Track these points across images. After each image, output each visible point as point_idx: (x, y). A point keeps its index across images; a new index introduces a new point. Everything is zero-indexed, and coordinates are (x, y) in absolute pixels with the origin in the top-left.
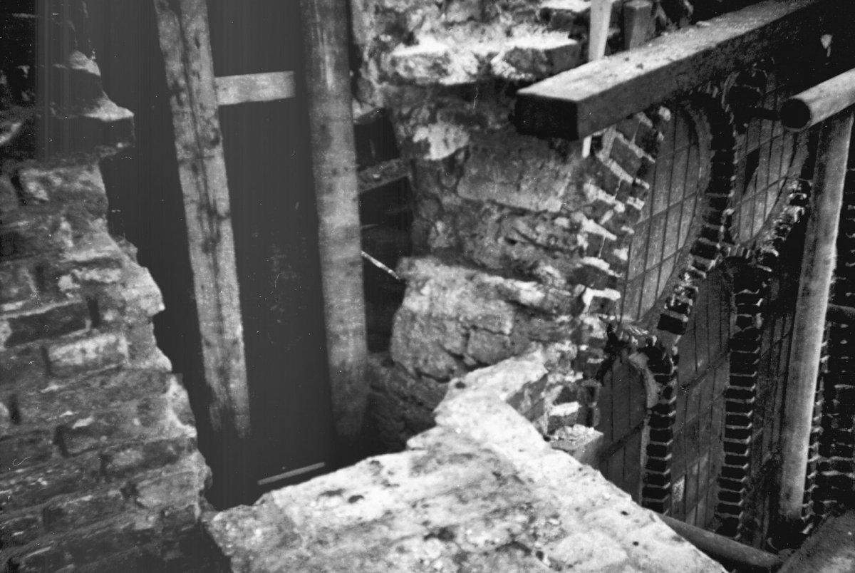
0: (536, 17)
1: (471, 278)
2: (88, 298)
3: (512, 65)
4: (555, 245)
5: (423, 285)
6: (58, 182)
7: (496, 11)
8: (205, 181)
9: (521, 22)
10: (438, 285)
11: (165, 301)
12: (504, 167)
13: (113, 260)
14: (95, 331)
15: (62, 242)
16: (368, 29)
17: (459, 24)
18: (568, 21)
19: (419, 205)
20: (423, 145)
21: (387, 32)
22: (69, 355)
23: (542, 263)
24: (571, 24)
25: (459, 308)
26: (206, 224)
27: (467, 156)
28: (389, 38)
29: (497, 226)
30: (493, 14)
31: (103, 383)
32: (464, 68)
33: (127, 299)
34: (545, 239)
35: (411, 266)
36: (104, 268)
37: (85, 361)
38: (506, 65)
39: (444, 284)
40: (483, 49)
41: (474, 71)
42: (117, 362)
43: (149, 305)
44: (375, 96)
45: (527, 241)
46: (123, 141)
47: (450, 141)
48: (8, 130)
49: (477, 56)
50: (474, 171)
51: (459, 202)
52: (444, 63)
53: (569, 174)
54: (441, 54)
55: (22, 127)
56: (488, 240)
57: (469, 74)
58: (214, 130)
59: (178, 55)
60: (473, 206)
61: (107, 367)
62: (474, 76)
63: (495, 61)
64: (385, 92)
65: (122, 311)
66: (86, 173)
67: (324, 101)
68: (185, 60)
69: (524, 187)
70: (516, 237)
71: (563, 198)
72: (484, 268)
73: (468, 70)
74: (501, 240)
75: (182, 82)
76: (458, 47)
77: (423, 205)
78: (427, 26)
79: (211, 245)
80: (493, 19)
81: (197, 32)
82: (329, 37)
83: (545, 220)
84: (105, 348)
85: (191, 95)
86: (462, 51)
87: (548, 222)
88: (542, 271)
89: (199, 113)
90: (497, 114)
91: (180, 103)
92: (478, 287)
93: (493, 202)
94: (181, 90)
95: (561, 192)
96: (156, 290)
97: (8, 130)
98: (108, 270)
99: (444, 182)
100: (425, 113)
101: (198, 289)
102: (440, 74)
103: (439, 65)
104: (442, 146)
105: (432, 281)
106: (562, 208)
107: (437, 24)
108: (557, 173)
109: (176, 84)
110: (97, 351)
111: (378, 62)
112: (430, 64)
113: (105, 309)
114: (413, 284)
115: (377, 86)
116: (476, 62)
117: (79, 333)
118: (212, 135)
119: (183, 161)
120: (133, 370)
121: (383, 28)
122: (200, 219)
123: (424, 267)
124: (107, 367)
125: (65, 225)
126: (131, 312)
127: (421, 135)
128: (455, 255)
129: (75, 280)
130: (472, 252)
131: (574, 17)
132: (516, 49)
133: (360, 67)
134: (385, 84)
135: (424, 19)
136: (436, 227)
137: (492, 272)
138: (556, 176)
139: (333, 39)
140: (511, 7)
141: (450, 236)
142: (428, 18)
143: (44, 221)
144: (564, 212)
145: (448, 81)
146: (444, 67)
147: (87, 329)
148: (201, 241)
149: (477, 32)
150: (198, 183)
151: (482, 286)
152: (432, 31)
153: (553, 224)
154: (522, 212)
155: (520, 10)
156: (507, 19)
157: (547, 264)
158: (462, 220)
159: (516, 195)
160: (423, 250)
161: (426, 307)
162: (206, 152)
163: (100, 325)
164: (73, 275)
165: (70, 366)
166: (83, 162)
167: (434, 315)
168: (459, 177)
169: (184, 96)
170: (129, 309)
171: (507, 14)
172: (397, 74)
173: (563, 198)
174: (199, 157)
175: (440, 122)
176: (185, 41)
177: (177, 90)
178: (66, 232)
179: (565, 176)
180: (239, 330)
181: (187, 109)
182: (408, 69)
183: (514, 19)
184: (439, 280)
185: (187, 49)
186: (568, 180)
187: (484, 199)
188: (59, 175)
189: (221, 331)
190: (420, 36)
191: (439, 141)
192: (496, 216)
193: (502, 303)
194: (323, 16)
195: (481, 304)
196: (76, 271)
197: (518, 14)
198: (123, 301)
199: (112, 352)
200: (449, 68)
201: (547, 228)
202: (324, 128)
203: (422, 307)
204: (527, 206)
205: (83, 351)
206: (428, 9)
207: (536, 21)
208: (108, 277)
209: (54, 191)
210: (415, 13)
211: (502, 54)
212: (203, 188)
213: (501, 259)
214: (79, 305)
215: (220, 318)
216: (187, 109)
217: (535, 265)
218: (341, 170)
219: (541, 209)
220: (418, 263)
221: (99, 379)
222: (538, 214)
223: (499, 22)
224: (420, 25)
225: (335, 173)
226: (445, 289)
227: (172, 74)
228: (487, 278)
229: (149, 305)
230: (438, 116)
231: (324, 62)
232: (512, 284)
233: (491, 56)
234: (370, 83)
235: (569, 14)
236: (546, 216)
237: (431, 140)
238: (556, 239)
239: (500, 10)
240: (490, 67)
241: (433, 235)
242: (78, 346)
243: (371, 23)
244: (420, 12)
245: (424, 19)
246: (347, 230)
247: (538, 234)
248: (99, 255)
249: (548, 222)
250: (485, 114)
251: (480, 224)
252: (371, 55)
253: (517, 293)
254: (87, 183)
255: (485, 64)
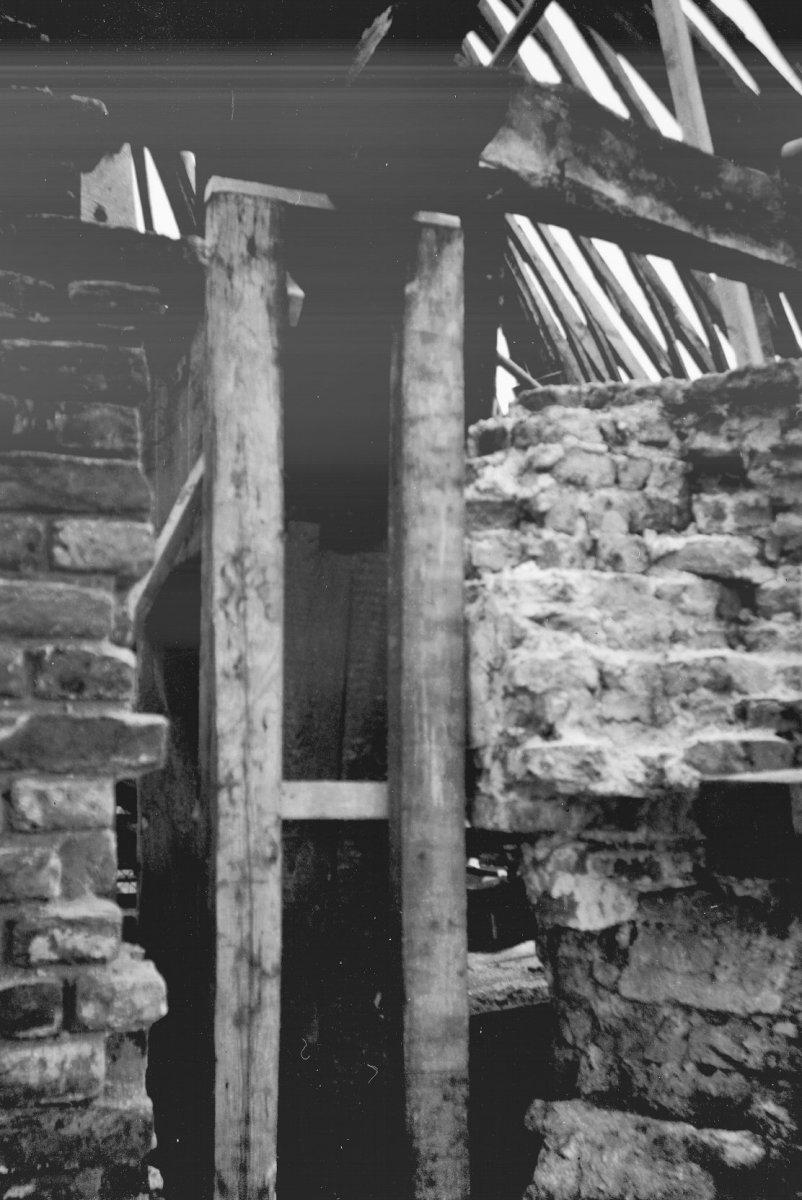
0: (728, 716)
1: (644, 1129)
2: (66, 982)
3: (696, 767)
4: (778, 1068)
5: (567, 1142)
6: (57, 798)
7: (671, 709)
8: (251, 915)
9: (707, 724)
10: (592, 1143)
11: (171, 999)
12: (688, 947)
13: (108, 923)
14: (66, 1035)
15: (47, 887)
16: (492, 722)
17: (619, 722)
18: (773, 714)
19: (561, 1021)
20: (566, 901)
21: (517, 725)
22: (22, 1064)
23: (757, 1097)
24: (778, 717)
25: (625, 1179)
26: (244, 982)
27: (634, 934)
28: (521, 731)
29: (684, 1045)
30: (667, 715)
31: (60, 1124)
32: (625, 773)
33: (118, 988)
34: (759, 1059)
35: (547, 1110)
36: (95, 933)
37: (42, 1079)
38: (685, 767)
39: (600, 1139)
40: (653, 751)
41: (640, 778)
42: (85, 1091)
43: (146, 1002)
44: (499, 814)
45: (731, 1067)
46: (148, 752)
47: (608, 907)
48: (12, 722)
49: (644, 760)
50: (644, 958)
51: (624, 1009)
52: (597, 762)
53: (791, 954)
54: (592, 749)
55: (31, 721)
56: (670, 1067)
57: (632, 781)
58: (273, 844)
59: (238, 740)
60: (608, 639)
61: (70, 1097)
62: (640, 786)
63: (668, 764)
64: (511, 806)
65: (106, 1004)
66: (96, 793)
67: (426, 820)
68: (246, 745)
69: (722, 977)
70: (715, 1061)
71: (783, 991)
72: (666, 1114)
73: (630, 776)
74: (690, 1067)
75: (238, 774)
76: (618, 750)
77: (567, 1020)
78: (573, 716)
79: (246, 1017)
80: (667, 722)
81: (267, 710)
82: (439, 736)
83: (758, 1028)
84: (74, 1063)
85: (247, 792)
86: (623, 755)
87: (764, 1032)
88: (759, 1111)
89: (254, 819)
90: (677, 862)
91: (232, 802)
92: (655, 1142)
93: (677, 1004)
94: (237, 784)
95: (781, 981)
96: (159, 981)
97: (12, 722)
98: (98, 936)
99: (599, 975)
100: (568, 853)
101: (219, 1086)
102: (592, 779)
103: (589, 765)
104: (595, 910)
105: (580, 1136)
106: (783, 1006)
107: (588, 716)
108: (773, 956)
109: (230, 776)
110: (61, 1065)
111: (504, 762)
112: (576, 762)
113: (86, 998)
114: (550, 1142)
115: (501, 799)
116: (643, 768)
117: (42, 1031)
118: (268, 851)
119: (225, 883)
120: (106, 1111)
121: (513, 717)
122: (236, 971)
123: (568, 1114)
124: (70, 1097)
125: (55, 862)
126: (122, 1010)
127: (563, 885)
128: (621, 1096)
129: (54, 945)
130: (645, 1090)
131: (782, 708)
132: (701, 744)
133: (480, 780)
134: (512, 795)
135: (569, 705)
136: (588, 1057)
137: (676, 1119)
138: (772, 958)
139: (445, 737)
140: (694, 704)
141: (611, 1069)
142: (574, 704)
143: (30, 853)
144: (787, 1013)
145: (601, 788)
146: (597, 768)
147: (53, 1028)
148: (234, 1008)
149: (644, 737)
150: (240, 918)
151: (660, 1141)
152: (581, 723)
153: (771, 1034)
154: (720, 1018)
155: (706, 707)
156: (687, 720)
157: (764, 1099)
158: (627, 1041)
159: (709, 991)
160: (565, 1087)
161: (571, 1182)
162: (257, 874)
163: (73, 1025)
164: (53, 939)
165: (20, 1085)
166: (92, 773)
167: (584, 1193)
168: (620, 967)
169: (237, 792)
170: (117, 1004)
171: (688, 714)
172: (530, 773)
173: (783, 991)
174: (247, 880)
175: (592, 873)
176: (250, 722)
177: (230, 784)
178: (54, 872)
179: (785, 957)
180: (272, 1169)
181: (240, 810)
182: (545, 765)
183: (697, 720)
184: (592, 1134)
185: (250, 731)
186: (789, 964)
187: (661, 999)
188: (61, 790)
189: (244, 1168)
190: (562, 729)
191: (593, 902)
192: (681, 1028)
193: (696, 1168)
194: (432, 705)
195: (661, 1170)
196: (57, 933)
197: (703, 713)
198: (113, 990)
199: (81, 1072)
200: (604, 771)
201: (762, 1043)
202: (422, 856)
203: (563, 1181)
204: (730, 1007)
205: (43, 1063)
206: (575, 693)
207: (730, 723)
208: (98, 948)
209: (50, 811)
210: (557, 696)
211: (681, 754)
212: (246, 927)
213: (690, 1099)
214: (52, 987)
215: (245, 1144)
216: (240, 810)
217: (748, 1101)
218: (445, 924)
219: (751, 1010)
220: (560, 1107)
221: (57, 1115)
222: (748, 1020)
223: (675, 724)
224: (564, 715)
225: (434, 925)
226: (601, 1148)
227: (227, 763)
228: (671, 1129)
229: (146, 1002)
230: (589, 864)
231: (430, 767)
232: (711, 1135)
233: (663, 757)
234: (491, 797)
235: (776, 705)
236: (760, 1021)
237: (578, 897)
238: (778, 1057)
239: (676, 708)
240: (662, 772)
241: (584, 1070)
242: (37, 1053)
243: (497, 714)
244: (564, 695)
245: (569, 705)
246: (450, 1022)
247: (748, 1052)
248: (91, 914)
249: (764, 1032)
250: (657, 859)
251: (656, 1043)
252: (494, 757)
253: (721, 1150)
254: (93, 806)
255: (656, 770)
